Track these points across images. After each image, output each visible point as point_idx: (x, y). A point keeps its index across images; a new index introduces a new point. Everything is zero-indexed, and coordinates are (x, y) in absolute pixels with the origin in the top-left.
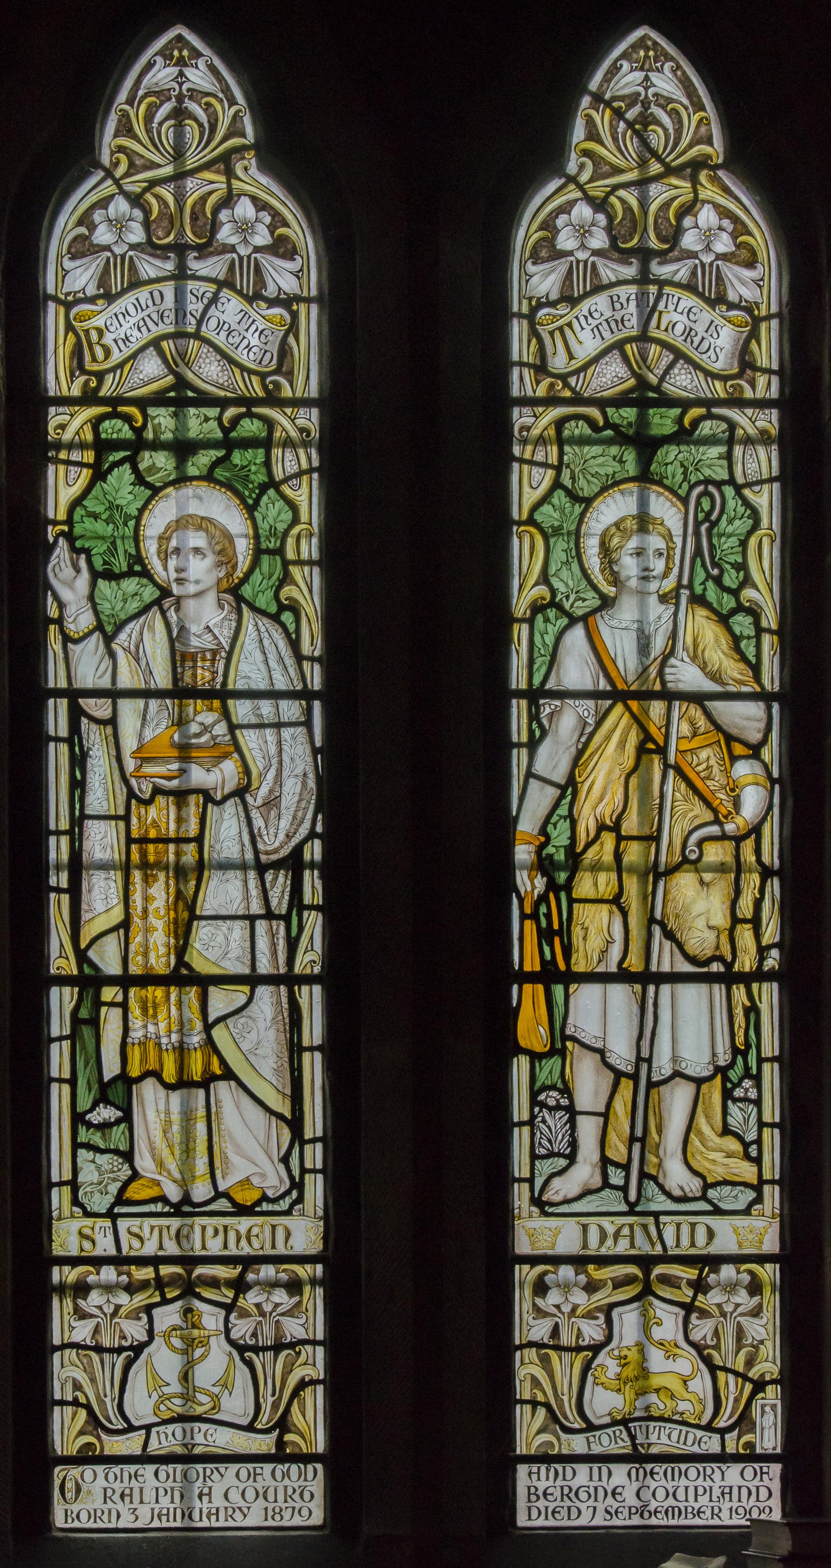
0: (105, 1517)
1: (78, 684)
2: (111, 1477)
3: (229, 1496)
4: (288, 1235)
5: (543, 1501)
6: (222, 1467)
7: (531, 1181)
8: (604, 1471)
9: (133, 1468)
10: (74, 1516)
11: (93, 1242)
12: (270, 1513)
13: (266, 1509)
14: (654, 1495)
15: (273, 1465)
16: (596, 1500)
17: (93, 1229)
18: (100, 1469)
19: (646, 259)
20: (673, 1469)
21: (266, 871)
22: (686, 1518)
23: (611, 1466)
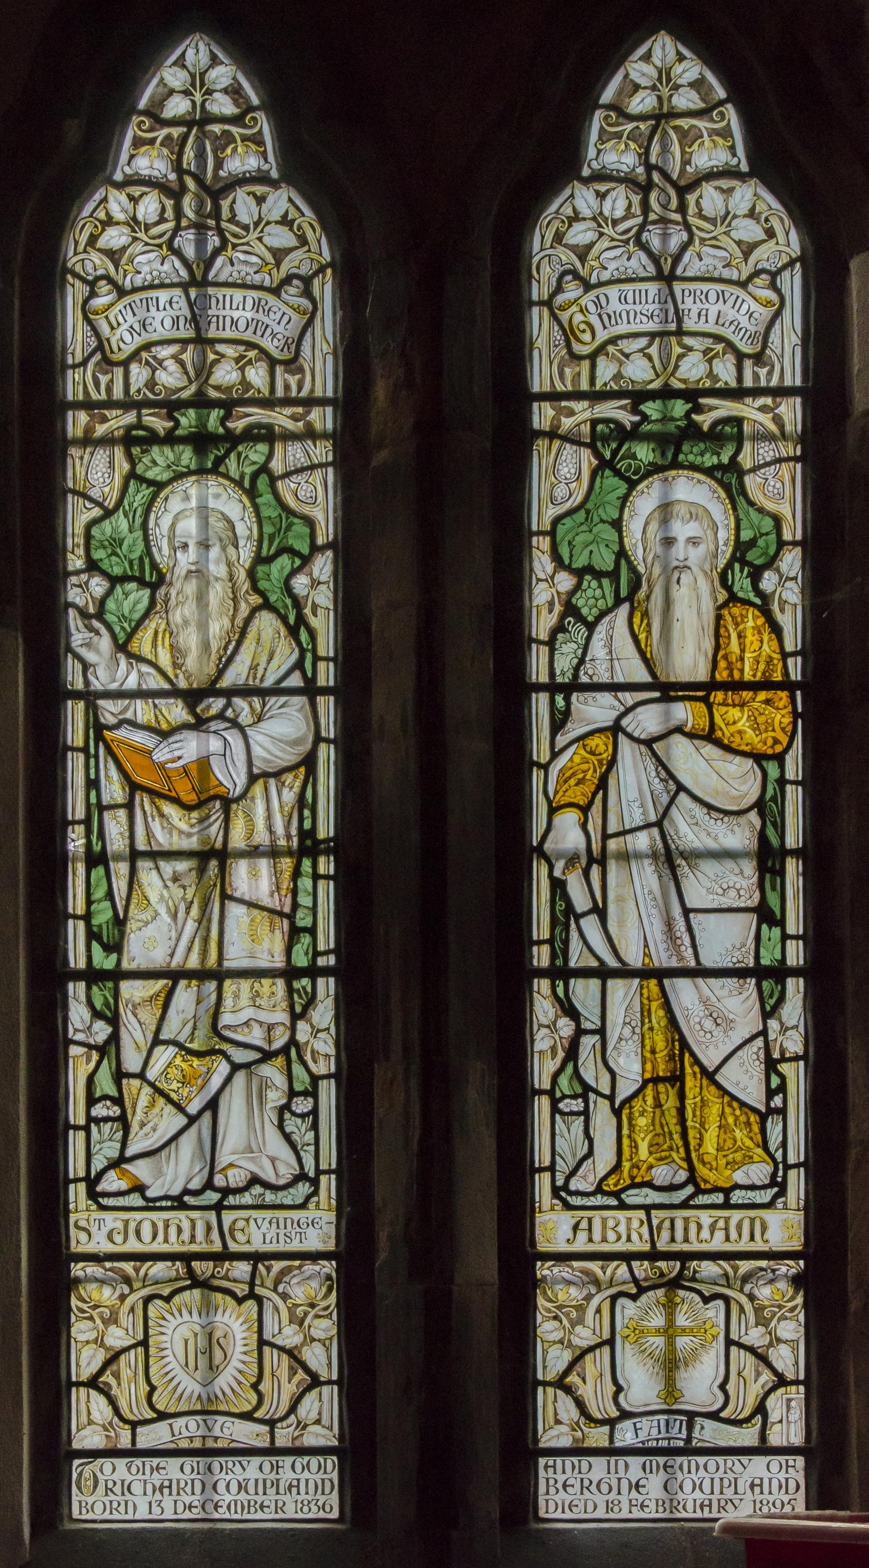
0: (122, 1509)
1: (96, 685)
3: (132, 1490)
5: (110, 1497)
6: (244, 1460)
7: (552, 1169)
8: (621, 1464)
9: (155, 1461)
10: (89, 1507)
11: (90, 1235)
12: (300, 1505)
13: (754, 1501)
14: (681, 1487)
15: (292, 1458)
17: (88, 1220)
20: (651, 1461)
21: (95, 866)
22: (249, 1512)
23: (591, 1459)
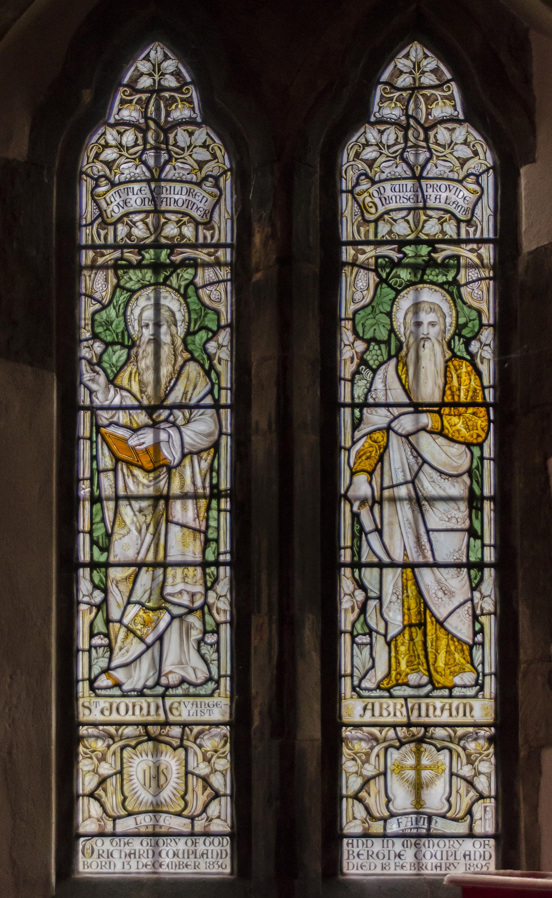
2: (114, 844)
4: (471, 709)
9: (127, 839)
12: (208, 865)
16: (389, 859)
18: (446, 840)
19: (420, 168)
